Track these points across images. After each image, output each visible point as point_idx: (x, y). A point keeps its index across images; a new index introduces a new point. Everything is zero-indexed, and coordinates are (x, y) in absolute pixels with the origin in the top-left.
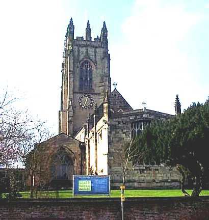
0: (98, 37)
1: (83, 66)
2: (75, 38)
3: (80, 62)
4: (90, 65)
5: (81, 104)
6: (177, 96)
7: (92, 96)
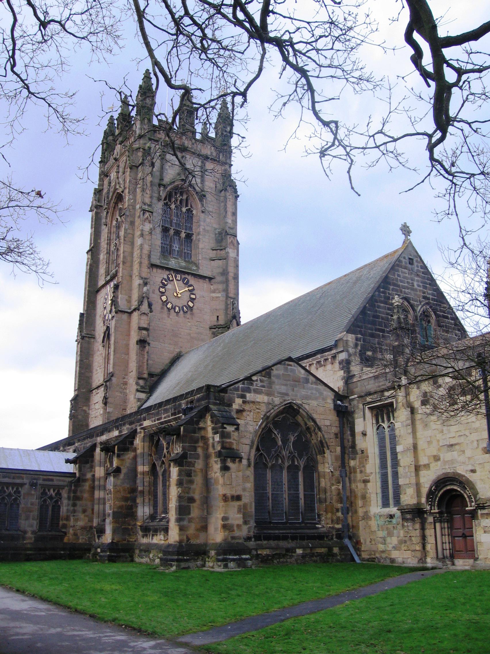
5: (164, 298)
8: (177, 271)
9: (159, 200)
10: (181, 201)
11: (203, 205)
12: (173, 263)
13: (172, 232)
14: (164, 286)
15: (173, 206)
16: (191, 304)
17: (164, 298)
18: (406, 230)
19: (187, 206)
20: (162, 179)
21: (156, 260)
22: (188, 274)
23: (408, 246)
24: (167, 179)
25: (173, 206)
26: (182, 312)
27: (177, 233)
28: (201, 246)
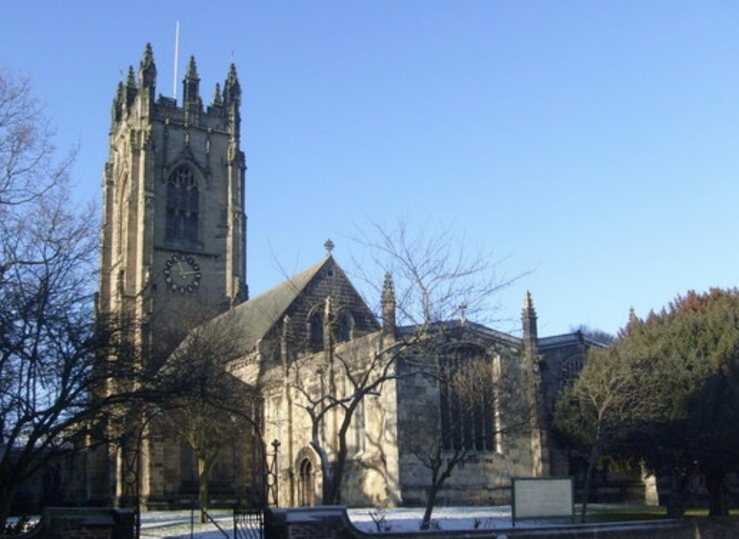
0: (73, 145)
1: (175, 180)
2: (157, 98)
3: (168, 168)
4: (192, 177)
5: (169, 280)
6: (529, 295)
7: (197, 260)
8: (182, 253)
9: (163, 182)
10: (186, 179)
11: (207, 183)
12: (177, 245)
13: (177, 213)
14: (169, 268)
15: (178, 186)
16: (196, 284)
17: (169, 280)
18: (329, 245)
19: (192, 182)
20: (165, 160)
21: (161, 244)
22: (193, 254)
23: (330, 262)
24: (171, 158)
25: (178, 186)
26: (187, 293)
27: (182, 212)
28: (206, 224)
